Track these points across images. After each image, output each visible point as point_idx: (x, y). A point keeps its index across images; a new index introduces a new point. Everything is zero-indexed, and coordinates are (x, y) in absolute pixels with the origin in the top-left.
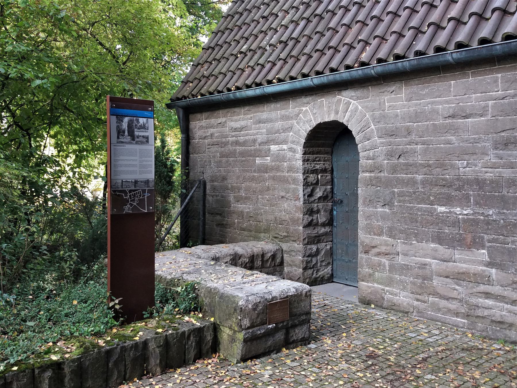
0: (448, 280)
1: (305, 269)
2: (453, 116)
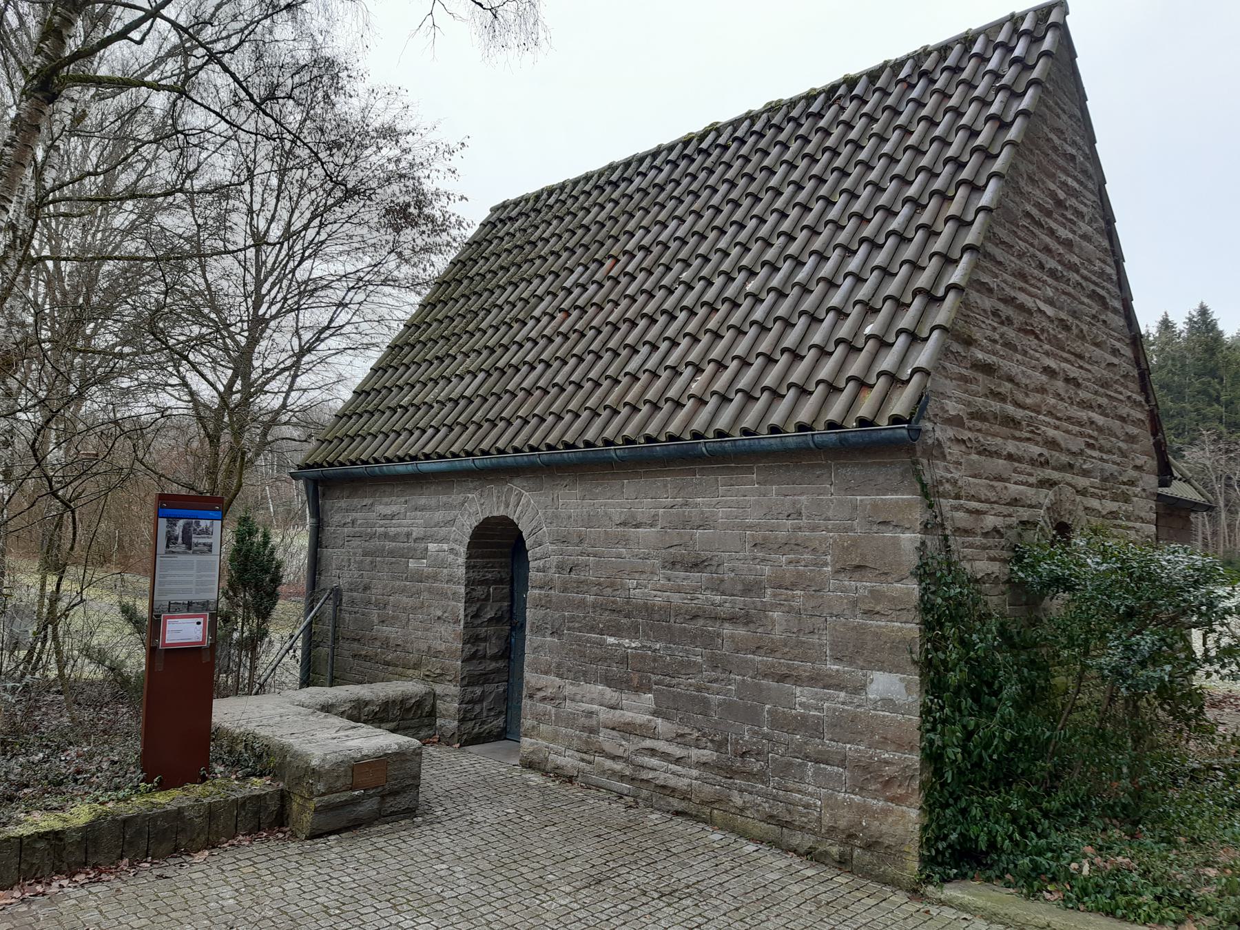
0: (614, 733)
1: (462, 721)
2: (624, 524)
